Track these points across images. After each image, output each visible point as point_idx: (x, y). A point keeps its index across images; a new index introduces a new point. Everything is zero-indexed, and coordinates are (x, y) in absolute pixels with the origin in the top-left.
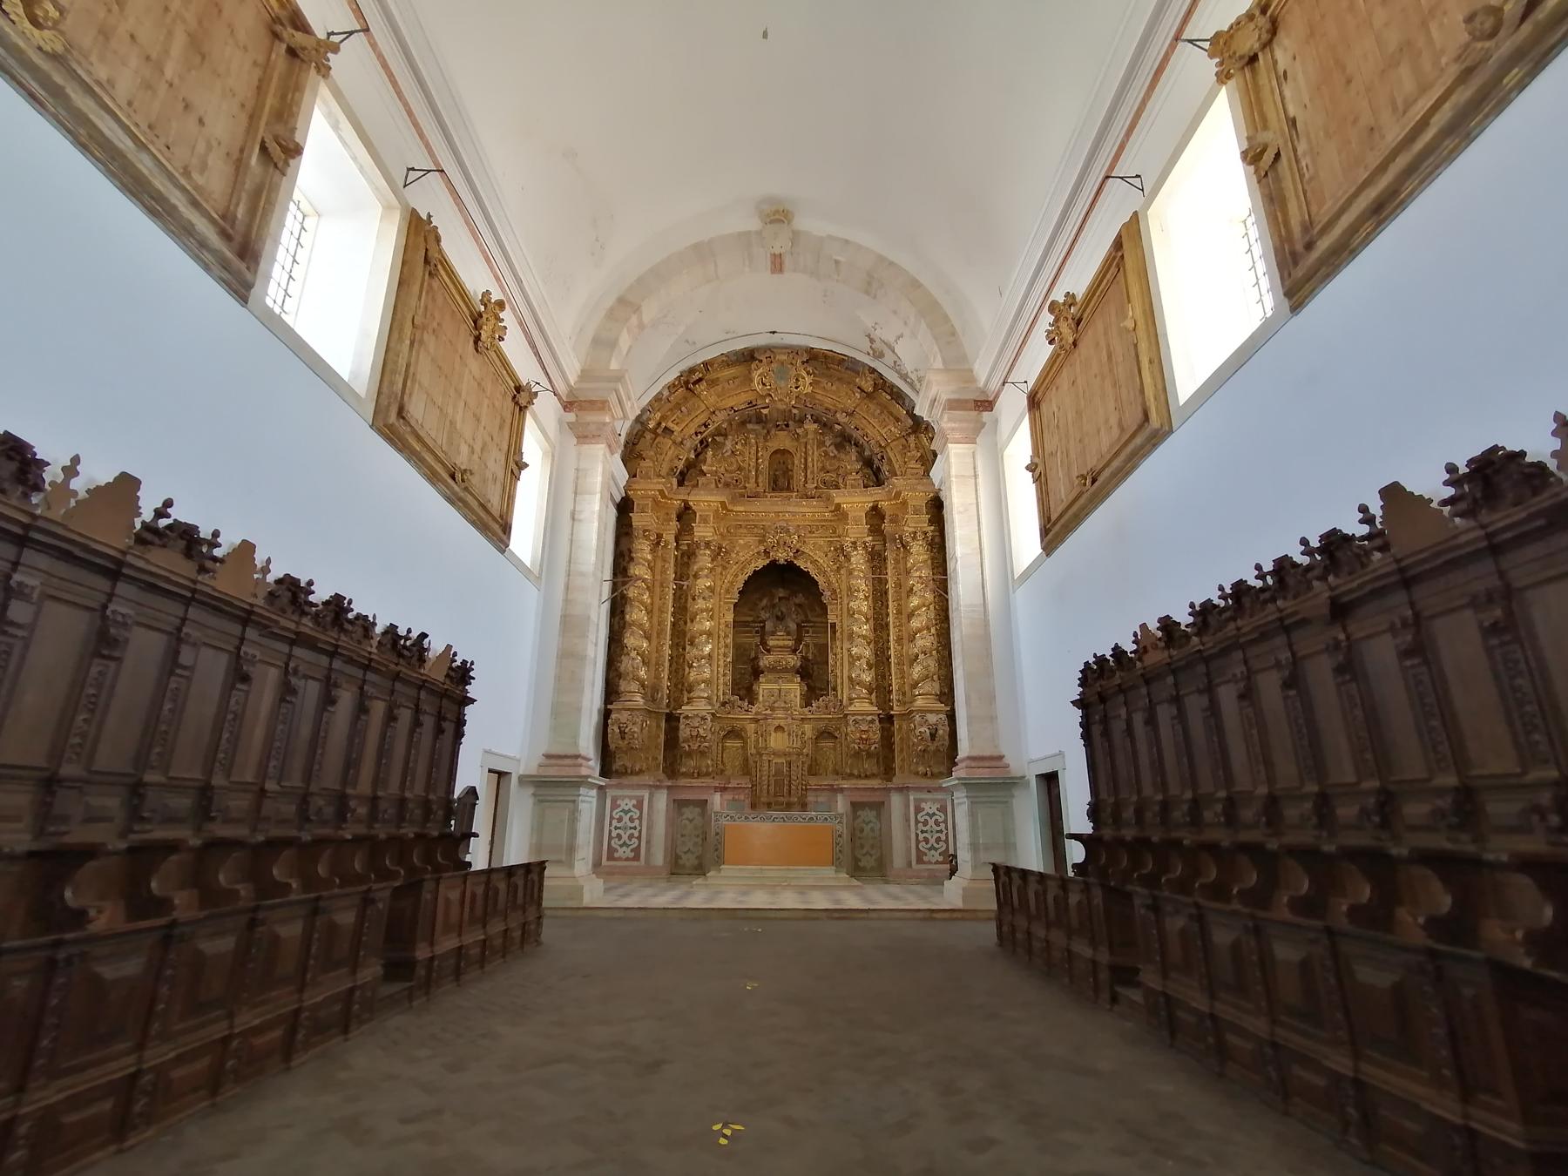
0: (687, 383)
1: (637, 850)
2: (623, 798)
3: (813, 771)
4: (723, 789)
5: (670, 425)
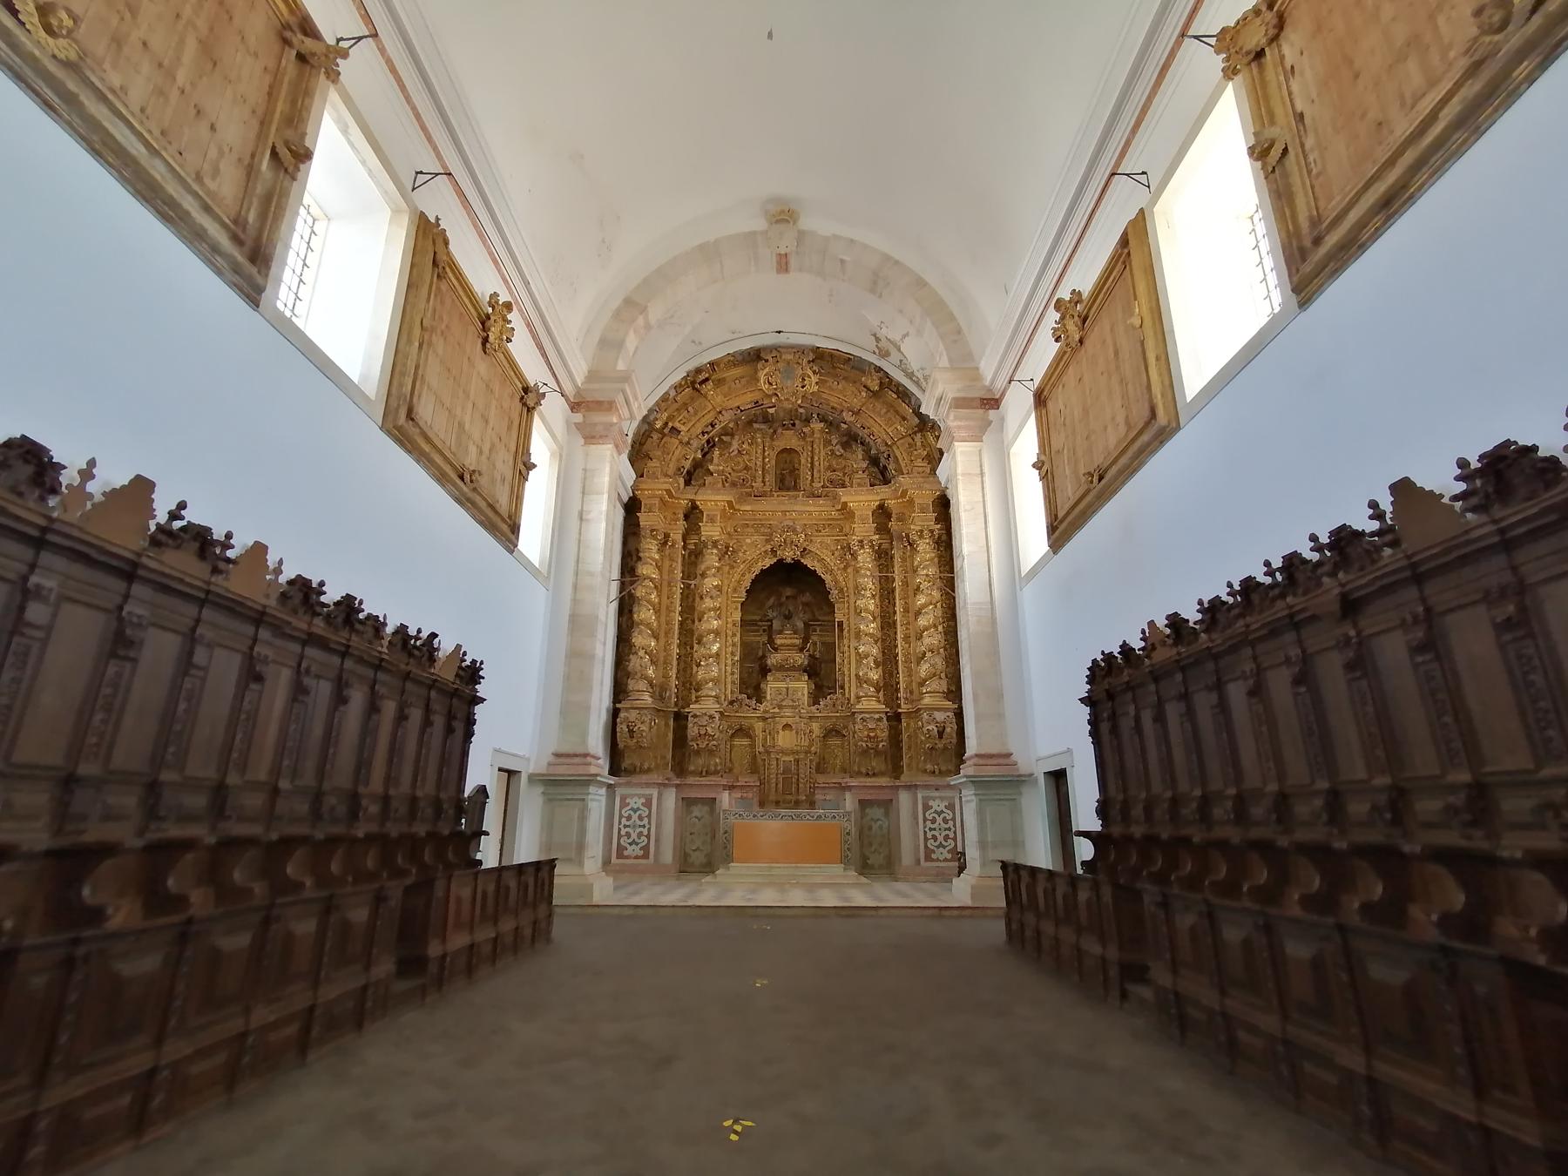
0: (693, 383)
1: (646, 848)
2: (632, 796)
4: (731, 788)
5: (677, 425)
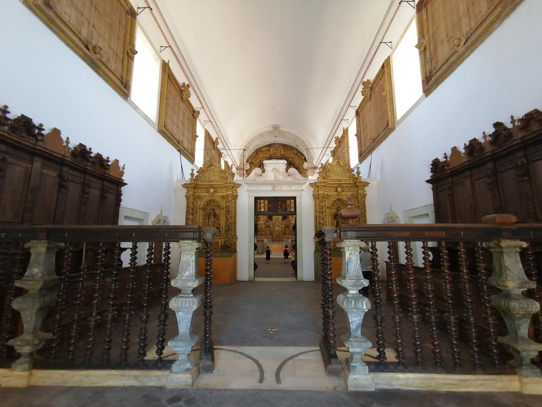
3: (284, 234)
